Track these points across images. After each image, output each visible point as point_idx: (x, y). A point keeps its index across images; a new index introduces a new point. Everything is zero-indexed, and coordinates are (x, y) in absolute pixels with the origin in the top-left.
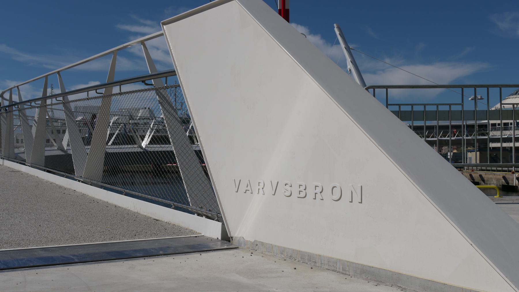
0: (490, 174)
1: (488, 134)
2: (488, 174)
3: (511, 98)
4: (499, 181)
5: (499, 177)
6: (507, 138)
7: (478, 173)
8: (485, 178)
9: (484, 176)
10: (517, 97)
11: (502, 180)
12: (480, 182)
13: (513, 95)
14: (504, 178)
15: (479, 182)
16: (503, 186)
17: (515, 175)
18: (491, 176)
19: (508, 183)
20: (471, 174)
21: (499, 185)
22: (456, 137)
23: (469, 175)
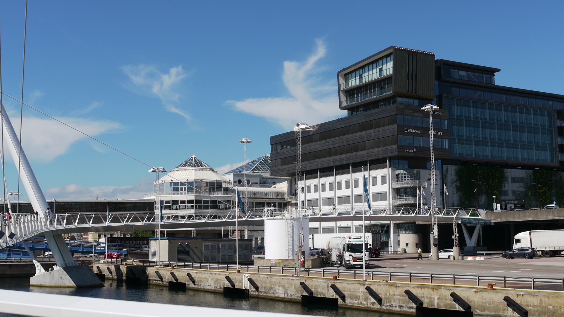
0: (204, 273)
1: (453, 239)
2: (201, 273)
3: (180, 170)
4: (220, 283)
5: (218, 277)
6: (185, 224)
7: (184, 270)
8: (195, 278)
9: (193, 275)
10: (187, 170)
11: (225, 280)
12: (187, 283)
13: (182, 167)
14: (172, 274)
15: (185, 284)
16: (226, 289)
17: (244, 275)
18: (206, 276)
19: (233, 285)
20: (454, 293)
21: (218, 288)
22: (152, 221)
23: (363, 289)
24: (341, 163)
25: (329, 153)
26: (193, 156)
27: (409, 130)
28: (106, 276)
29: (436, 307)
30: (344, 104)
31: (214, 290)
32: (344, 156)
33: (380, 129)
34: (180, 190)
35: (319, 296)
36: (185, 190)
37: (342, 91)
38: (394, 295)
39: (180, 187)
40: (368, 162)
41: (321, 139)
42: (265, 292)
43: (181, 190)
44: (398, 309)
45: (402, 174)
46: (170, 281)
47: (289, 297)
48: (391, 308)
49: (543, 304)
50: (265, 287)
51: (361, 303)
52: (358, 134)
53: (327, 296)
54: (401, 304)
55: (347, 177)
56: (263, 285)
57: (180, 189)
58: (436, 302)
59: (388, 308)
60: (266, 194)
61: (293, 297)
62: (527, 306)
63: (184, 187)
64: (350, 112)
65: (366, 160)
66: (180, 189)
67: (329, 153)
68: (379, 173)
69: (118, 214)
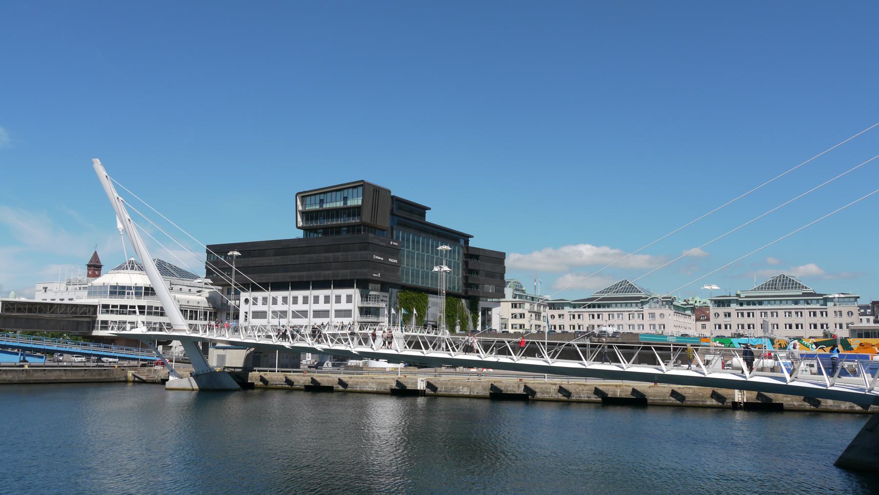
24: (301, 280)
25: (285, 268)
26: (132, 259)
27: (377, 257)
28: (334, 388)
29: (618, 396)
30: (300, 224)
31: (476, 395)
32: (304, 273)
33: (349, 253)
34: (126, 294)
35: (509, 393)
36: (132, 294)
37: (300, 211)
38: (583, 390)
39: (127, 291)
40: (355, 282)
41: (275, 255)
42: (446, 392)
43: (127, 295)
44: (586, 399)
45: (375, 295)
46: (162, 378)
47: (475, 394)
48: (580, 399)
49: (696, 393)
50: (445, 388)
51: (552, 396)
52: (323, 255)
53: (517, 393)
54: (589, 396)
55: (306, 293)
56: (444, 386)
57: (126, 293)
58: (618, 394)
59: (578, 398)
60: (188, 302)
61: (480, 394)
62: (686, 394)
63: (131, 291)
64: (305, 231)
65: (331, 279)
66: (126, 293)
67: (285, 268)
68: (344, 293)
69: (509, 342)
